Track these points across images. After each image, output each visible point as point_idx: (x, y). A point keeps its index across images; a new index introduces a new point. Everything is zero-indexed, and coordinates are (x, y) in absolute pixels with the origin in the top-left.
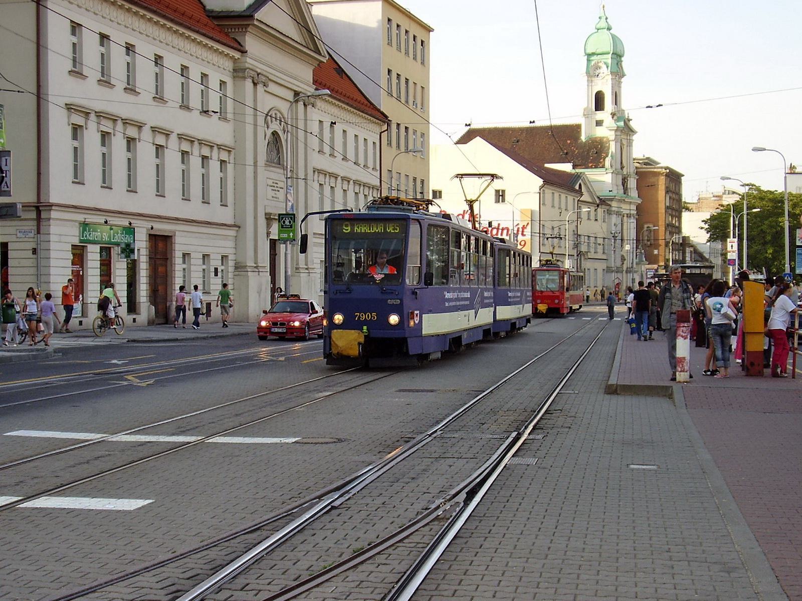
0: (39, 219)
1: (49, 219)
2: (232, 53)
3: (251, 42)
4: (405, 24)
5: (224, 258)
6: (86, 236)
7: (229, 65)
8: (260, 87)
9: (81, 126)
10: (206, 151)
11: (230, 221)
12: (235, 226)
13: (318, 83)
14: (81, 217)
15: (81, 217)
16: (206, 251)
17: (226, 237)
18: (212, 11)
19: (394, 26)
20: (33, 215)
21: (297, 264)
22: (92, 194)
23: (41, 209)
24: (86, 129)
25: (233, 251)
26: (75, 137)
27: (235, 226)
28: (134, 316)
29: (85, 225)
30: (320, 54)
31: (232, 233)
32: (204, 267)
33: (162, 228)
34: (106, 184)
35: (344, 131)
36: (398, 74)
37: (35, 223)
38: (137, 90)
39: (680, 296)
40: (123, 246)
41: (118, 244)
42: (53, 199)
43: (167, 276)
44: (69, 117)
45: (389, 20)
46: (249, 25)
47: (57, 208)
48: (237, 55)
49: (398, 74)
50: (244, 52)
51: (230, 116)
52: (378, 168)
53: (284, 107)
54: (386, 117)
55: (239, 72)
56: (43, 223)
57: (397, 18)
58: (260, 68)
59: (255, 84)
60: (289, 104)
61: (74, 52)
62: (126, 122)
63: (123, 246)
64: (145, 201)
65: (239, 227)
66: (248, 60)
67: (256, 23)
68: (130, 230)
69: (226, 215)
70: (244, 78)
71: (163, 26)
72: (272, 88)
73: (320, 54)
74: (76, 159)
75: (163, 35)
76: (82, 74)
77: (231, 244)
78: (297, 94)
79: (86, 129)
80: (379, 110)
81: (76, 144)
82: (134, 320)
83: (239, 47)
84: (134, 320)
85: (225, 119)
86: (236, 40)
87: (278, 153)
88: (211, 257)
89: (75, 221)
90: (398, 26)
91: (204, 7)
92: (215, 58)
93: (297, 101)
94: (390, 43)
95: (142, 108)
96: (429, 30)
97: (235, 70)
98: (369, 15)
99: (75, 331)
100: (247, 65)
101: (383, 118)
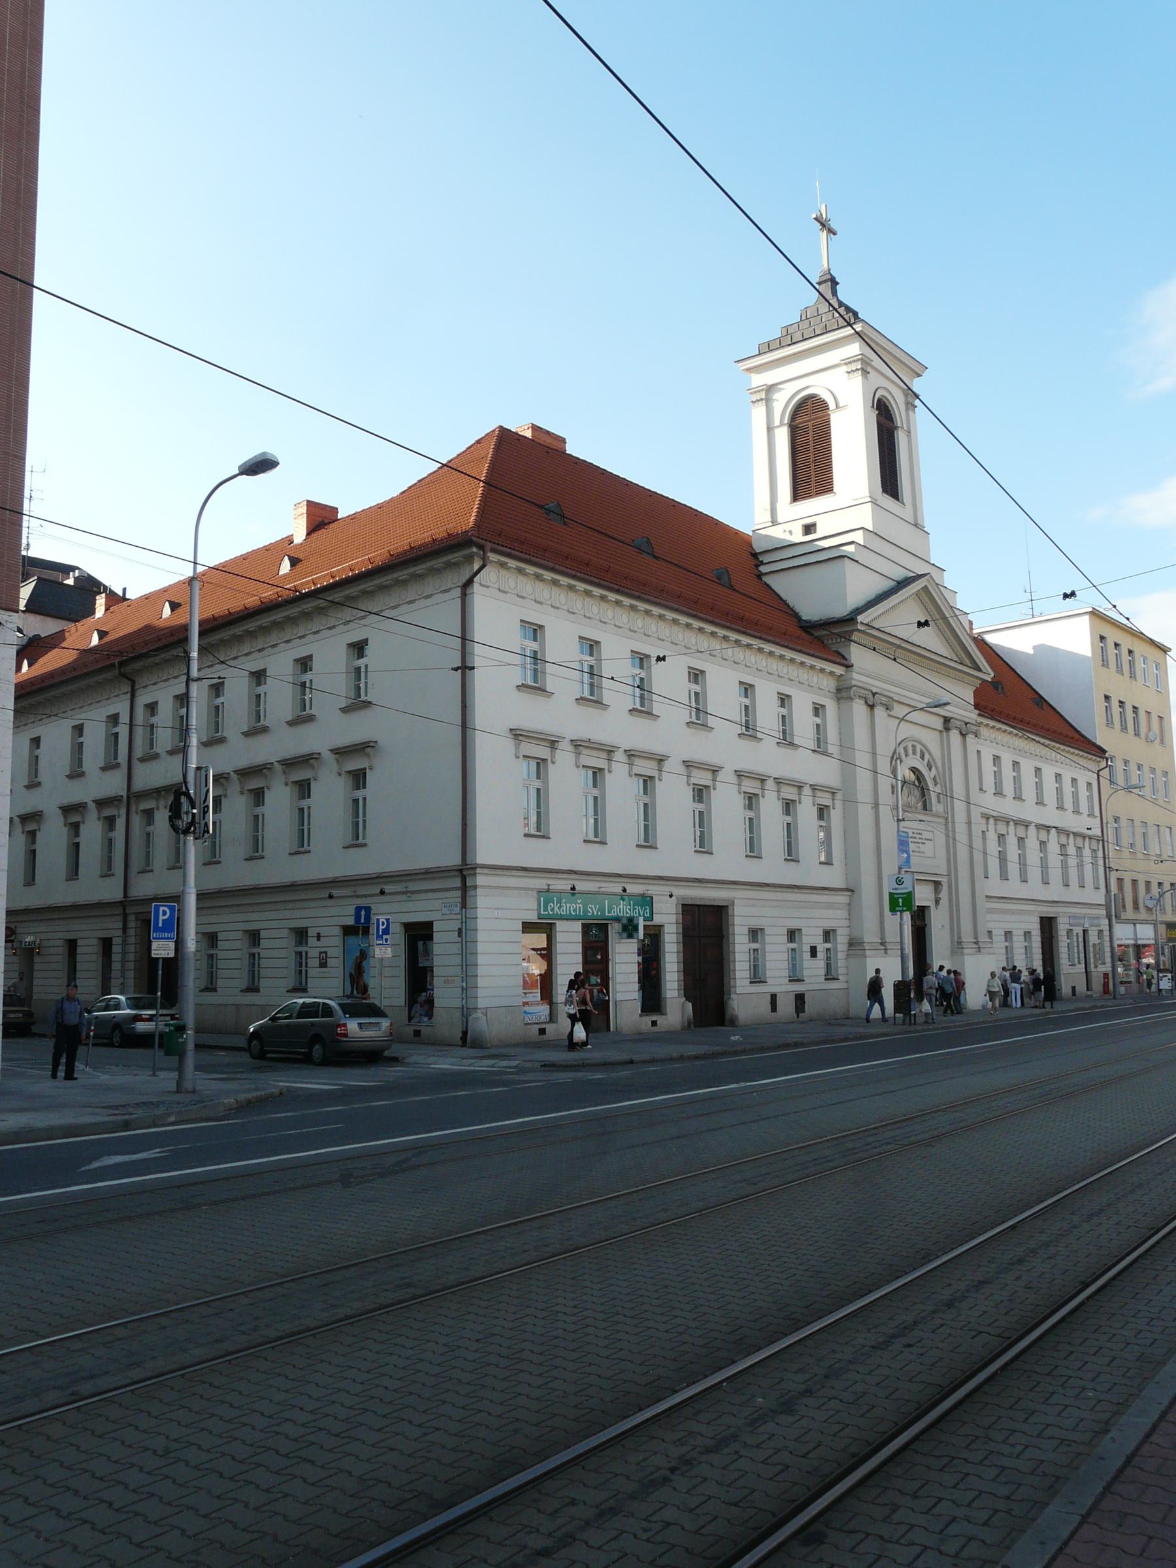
0: (464, 889)
1: (475, 887)
2: (829, 667)
3: (857, 654)
4: (1126, 642)
5: (828, 935)
6: (552, 910)
7: (829, 684)
8: (879, 712)
9: (707, 787)
10: (1002, 828)
11: (841, 885)
12: (847, 890)
13: (980, 706)
14: (540, 883)
15: (540, 883)
16: (1008, 927)
17: (830, 906)
18: (809, 622)
19: (1111, 646)
20: (457, 883)
21: (959, 937)
22: (566, 849)
23: (465, 873)
24: (553, 763)
25: (846, 923)
26: (787, 812)
27: (847, 890)
28: (654, 1018)
29: (546, 894)
30: (980, 670)
31: (842, 899)
32: (755, 946)
33: (1048, 911)
34: (1004, 876)
35: (978, 752)
36: (1120, 702)
37: (459, 893)
38: (759, 735)
39: (745, 948)
40: (625, 921)
41: (617, 919)
42: (480, 860)
43: (722, 959)
44: (517, 747)
45: (1102, 638)
46: (852, 631)
47: (486, 871)
48: (839, 670)
49: (1120, 702)
50: (849, 666)
51: (832, 749)
52: (1097, 813)
53: (931, 740)
54: (1104, 751)
55: (843, 693)
56: (470, 893)
57: (1113, 635)
58: (876, 685)
59: (963, 735)
60: (937, 734)
61: (784, 724)
62: (1017, 823)
63: (625, 921)
64: (675, 856)
65: (853, 891)
66: (855, 676)
67: (860, 627)
68: (646, 901)
69: (833, 877)
70: (851, 699)
71: (1010, 733)
72: (899, 711)
73: (980, 670)
74: (789, 836)
75: (784, 669)
76: (651, 714)
77: (842, 914)
78: (947, 720)
79: (553, 763)
80: (1094, 745)
81: (789, 819)
82: (654, 1023)
83: (843, 662)
84: (654, 1023)
85: (825, 753)
86: (839, 653)
87: (923, 795)
88: (804, 932)
89: (532, 889)
90: (1116, 645)
91: (796, 616)
92: (804, 675)
93: (947, 729)
94: (1105, 663)
95: (1028, 811)
96: (1164, 650)
97: (839, 690)
98: (1075, 638)
99: (492, 1047)
100: (854, 683)
101: (1100, 752)
